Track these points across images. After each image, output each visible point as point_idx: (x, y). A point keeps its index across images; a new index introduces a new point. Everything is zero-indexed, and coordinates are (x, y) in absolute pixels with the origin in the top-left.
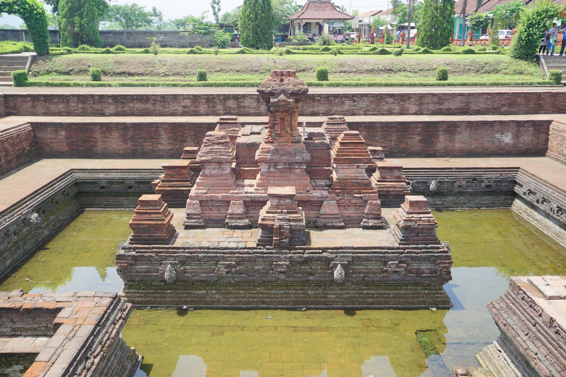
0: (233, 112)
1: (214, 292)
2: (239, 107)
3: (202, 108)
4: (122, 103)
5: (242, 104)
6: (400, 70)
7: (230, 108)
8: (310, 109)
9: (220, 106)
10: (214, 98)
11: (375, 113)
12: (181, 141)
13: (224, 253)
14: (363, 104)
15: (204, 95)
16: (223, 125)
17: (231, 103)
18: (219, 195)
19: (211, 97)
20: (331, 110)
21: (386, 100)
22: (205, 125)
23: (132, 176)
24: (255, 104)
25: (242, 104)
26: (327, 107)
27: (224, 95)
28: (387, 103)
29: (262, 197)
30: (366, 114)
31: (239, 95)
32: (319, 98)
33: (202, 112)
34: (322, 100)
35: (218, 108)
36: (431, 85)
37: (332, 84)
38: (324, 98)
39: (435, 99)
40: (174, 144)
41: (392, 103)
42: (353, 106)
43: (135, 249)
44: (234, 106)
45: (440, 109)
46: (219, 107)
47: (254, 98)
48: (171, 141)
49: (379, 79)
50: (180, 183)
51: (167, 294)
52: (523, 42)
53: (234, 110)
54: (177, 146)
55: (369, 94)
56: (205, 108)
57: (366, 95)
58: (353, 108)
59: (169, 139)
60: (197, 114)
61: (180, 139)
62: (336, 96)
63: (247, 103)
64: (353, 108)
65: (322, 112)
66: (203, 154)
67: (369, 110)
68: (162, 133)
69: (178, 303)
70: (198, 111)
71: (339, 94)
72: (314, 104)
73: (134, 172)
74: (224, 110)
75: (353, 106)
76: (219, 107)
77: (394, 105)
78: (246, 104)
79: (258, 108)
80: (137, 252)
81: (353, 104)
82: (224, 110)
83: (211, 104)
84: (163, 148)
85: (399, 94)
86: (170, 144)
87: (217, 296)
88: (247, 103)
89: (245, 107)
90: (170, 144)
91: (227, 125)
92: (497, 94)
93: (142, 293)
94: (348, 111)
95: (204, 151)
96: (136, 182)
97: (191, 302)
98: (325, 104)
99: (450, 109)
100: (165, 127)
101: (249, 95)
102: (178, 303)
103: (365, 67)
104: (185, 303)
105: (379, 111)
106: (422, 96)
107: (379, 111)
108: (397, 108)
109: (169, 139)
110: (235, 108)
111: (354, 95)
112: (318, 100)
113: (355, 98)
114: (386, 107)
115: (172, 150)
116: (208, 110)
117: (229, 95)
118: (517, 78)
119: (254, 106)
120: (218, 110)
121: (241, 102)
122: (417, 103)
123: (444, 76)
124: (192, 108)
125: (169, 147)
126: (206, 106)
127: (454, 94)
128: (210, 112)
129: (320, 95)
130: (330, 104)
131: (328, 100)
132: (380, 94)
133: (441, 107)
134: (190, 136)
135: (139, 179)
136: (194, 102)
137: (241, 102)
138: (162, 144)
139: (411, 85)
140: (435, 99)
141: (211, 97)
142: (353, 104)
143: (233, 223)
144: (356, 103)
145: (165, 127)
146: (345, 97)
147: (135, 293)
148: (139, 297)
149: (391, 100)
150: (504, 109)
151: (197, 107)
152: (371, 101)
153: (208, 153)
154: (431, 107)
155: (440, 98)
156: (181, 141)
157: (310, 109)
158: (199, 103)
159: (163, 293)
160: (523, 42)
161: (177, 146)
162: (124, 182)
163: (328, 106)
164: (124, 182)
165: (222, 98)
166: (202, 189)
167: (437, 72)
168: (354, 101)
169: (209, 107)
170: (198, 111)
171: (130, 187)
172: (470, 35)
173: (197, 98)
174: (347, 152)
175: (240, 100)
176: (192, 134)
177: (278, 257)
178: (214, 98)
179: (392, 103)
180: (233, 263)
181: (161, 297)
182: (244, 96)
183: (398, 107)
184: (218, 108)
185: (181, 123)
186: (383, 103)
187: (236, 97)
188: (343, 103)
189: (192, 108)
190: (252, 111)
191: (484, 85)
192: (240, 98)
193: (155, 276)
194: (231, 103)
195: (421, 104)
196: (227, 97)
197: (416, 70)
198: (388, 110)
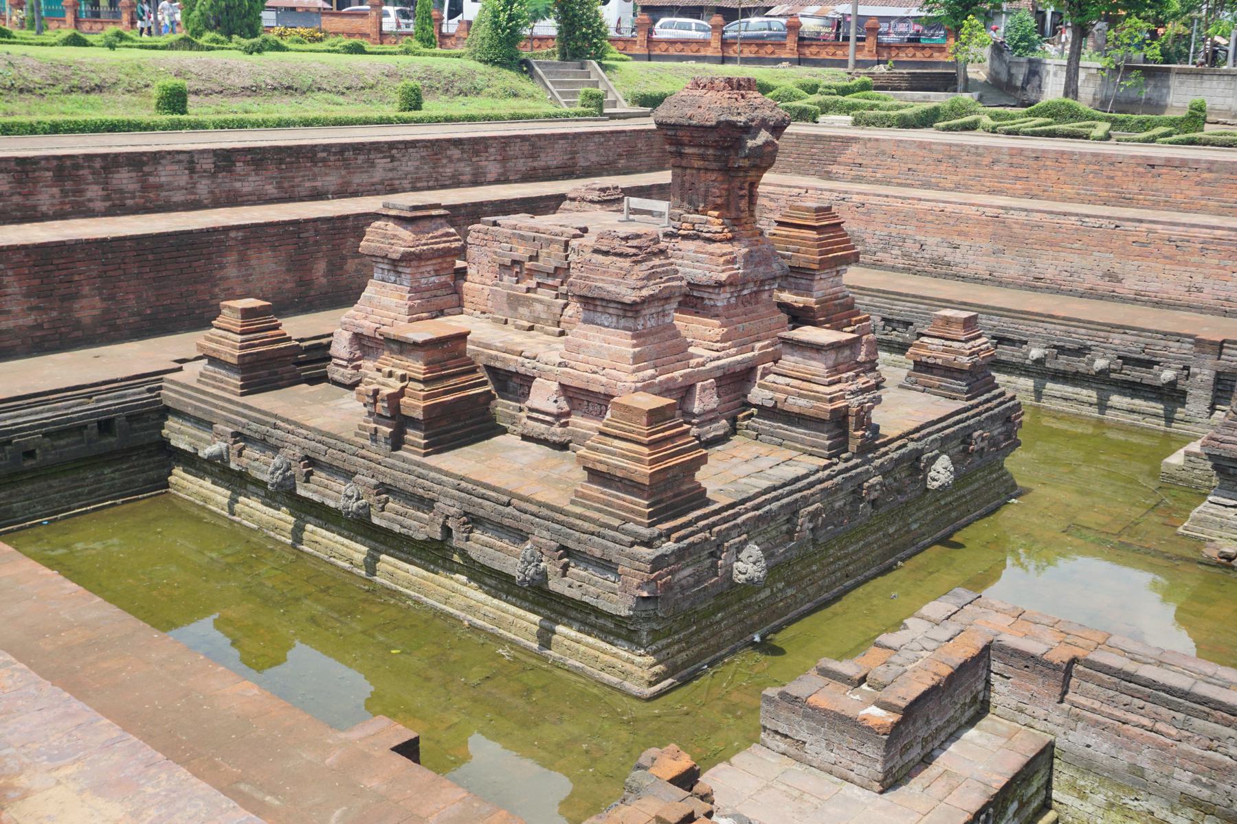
0: (129, 202)
1: (781, 585)
2: (145, 188)
3: (46, 197)
4: (226, 172)
5: (152, 179)
6: (310, 89)
7: (121, 191)
8: (308, 184)
9: (95, 187)
10: (77, 167)
11: (431, 184)
12: (64, 298)
13: (800, 490)
14: (409, 165)
15: (47, 158)
16: (421, 224)
17: (124, 179)
18: (676, 374)
19: (68, 163)
20: (349, 183)
21: (449, 153)
22: (128, 243)
23: (27, 417)
24: (183, 179)
25: (152, 179)
26: (343, 177)
27: (104, 156)
28: (450, 159)
29: (739, 362)
30: (415, 189)
31: (144, 154)
32: (325, 154)
33: (44, 208)
34: (332, 158)
35: (89, 195)
36: (387, 121)
37: (225, 121)
38: (335, 154)
39: (526, 147)
40: (44, 310)
41: (459, 160)
42: (391, 170)
43: (667, 535)
44: (131, 187)
45: (535, 169)
46: (93, 191)
47: (180, 161)
48: (34, 301)
49: (259, 109)
50: (464, 378)
51: (718, 623)
52: (503, 31)
53: (133, 198)
54: (54, 314)
55: (418, 141)
56: (53, 196)
57: (413, 144)
58: (390, 175)
59: (28, 295)
60: (31, 215)
61: (62, 291)
62: (358, 148)
63: (165, 175)
64: (390, 175)
65: (332, 188)
66: (640, 284)
67: (419, 179)
68: (6, 280)
69: (741, 635)
70: (34, 207)
71: (363, 144)
72: (316, 170)
73: (30, 406)
74: (107, 198)
75: (391, 170)
76: (93, 191)
77: (462, 164)
78: (163, 179)
79: (191, 188)
80: (678, 540)
81: (390, 165)
82: (107, 198)
83: (69, 185)
84: (11, 324)
85: (469, 139)
86: (31, 309)
87: (790, 592)
88: (165, 175)
89: (159, 187)
90: (31, 309)
91: (427, 223)
92: (612, 132)
93: (680, 641)
94: (382, 183)
95: (642, 275)
96: (45, 435)
97: (764, 621)
98: (338, 168)
99: (549, 168)
100: (16, 258)
101: (169, 153)
102: (741, 635)
103: (238, 81)
104: (753, 629)
105: (437, 180)
106: (506, 141)
107: (437, 180)
108: (467, 170)
109: (28, 295)
110: (133, 193)
111: (392, 145)
112: (324, 160)
113: (394, 151)
114: (449, 171)
115: (39, 326)
116: (63, 203)
117: (117, 155)
118: (506, 106)
119: (183, 183)
120: (90, 200)
121: (150, 174)
122: (499, 158)
123: (413, 100)
124: (17, 199)
125: (30, 320)
126: (55, 190)
127: (553, 135)
128: (67, 208)
129: (327, 148)
130: (347, 167)
131: (344, 160)
132: (437, 140)
133: (535, 164)
134: (89, 278)
135: (54, 423)
136: (19, 182)
137: (150, 174)
138: (9, 312)
139: (55, 129)
140: (526, 147)
141: (68, 163)
142: (390, 165)
143: (708, 432)
144: (396, 164)
145: (16, 258)
146: (376, 149)
147: (669, 646)
148: (679, 651)
149: (455, 153)
150: (622, 163)
151: (31, 194)
152: (423, 158)
153: (648, 278)
154: (522, 165)
155: (533, 146)
156: (64, 298)
157: (308, 184)
158: (36, 181)
159: (712, 624)
160: (503, 31)
161: (54, 314)
162: (9, 442)
163: (343, 172)
164: (9, 442)
165: (98, 164)
166: (645, 368)
167: (155, 92)
168: (393, 159)
169: (64, 193)
170: (34, 207)
171: (30, 454)
172: (129, 11)
173: (28, 167)
174: (829, 244)
175: (146, 169)
176: (95, 274)
177: (867, 471)
178: (77, 167)
179: (459, 160)
180: (818, 505)
181: (714, 635)
182: (156, 157)
183: (468, 169)
184: (89, 195)
185: (64, 242)
186: (444, 161)
187: (136, 161)
188: (373, 165)
189: (17, 199)
190: (178, 197)
191: (499, 119)
192: (145, 164)
193: (712, 585)
194: (124, 179)
195: (505, 160)
196: (111, 162)
197: (341, 88)
198: (453, 176)
